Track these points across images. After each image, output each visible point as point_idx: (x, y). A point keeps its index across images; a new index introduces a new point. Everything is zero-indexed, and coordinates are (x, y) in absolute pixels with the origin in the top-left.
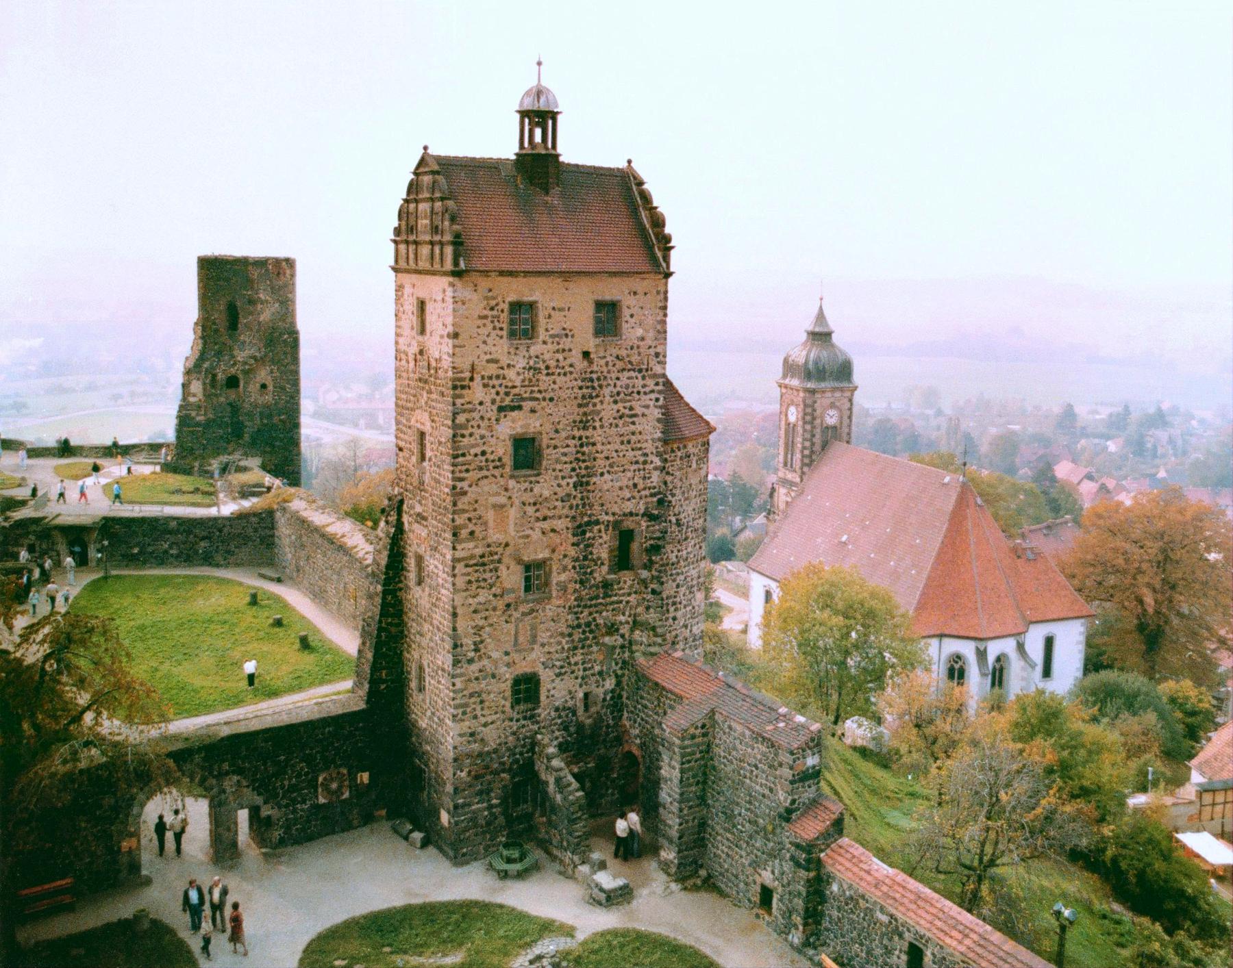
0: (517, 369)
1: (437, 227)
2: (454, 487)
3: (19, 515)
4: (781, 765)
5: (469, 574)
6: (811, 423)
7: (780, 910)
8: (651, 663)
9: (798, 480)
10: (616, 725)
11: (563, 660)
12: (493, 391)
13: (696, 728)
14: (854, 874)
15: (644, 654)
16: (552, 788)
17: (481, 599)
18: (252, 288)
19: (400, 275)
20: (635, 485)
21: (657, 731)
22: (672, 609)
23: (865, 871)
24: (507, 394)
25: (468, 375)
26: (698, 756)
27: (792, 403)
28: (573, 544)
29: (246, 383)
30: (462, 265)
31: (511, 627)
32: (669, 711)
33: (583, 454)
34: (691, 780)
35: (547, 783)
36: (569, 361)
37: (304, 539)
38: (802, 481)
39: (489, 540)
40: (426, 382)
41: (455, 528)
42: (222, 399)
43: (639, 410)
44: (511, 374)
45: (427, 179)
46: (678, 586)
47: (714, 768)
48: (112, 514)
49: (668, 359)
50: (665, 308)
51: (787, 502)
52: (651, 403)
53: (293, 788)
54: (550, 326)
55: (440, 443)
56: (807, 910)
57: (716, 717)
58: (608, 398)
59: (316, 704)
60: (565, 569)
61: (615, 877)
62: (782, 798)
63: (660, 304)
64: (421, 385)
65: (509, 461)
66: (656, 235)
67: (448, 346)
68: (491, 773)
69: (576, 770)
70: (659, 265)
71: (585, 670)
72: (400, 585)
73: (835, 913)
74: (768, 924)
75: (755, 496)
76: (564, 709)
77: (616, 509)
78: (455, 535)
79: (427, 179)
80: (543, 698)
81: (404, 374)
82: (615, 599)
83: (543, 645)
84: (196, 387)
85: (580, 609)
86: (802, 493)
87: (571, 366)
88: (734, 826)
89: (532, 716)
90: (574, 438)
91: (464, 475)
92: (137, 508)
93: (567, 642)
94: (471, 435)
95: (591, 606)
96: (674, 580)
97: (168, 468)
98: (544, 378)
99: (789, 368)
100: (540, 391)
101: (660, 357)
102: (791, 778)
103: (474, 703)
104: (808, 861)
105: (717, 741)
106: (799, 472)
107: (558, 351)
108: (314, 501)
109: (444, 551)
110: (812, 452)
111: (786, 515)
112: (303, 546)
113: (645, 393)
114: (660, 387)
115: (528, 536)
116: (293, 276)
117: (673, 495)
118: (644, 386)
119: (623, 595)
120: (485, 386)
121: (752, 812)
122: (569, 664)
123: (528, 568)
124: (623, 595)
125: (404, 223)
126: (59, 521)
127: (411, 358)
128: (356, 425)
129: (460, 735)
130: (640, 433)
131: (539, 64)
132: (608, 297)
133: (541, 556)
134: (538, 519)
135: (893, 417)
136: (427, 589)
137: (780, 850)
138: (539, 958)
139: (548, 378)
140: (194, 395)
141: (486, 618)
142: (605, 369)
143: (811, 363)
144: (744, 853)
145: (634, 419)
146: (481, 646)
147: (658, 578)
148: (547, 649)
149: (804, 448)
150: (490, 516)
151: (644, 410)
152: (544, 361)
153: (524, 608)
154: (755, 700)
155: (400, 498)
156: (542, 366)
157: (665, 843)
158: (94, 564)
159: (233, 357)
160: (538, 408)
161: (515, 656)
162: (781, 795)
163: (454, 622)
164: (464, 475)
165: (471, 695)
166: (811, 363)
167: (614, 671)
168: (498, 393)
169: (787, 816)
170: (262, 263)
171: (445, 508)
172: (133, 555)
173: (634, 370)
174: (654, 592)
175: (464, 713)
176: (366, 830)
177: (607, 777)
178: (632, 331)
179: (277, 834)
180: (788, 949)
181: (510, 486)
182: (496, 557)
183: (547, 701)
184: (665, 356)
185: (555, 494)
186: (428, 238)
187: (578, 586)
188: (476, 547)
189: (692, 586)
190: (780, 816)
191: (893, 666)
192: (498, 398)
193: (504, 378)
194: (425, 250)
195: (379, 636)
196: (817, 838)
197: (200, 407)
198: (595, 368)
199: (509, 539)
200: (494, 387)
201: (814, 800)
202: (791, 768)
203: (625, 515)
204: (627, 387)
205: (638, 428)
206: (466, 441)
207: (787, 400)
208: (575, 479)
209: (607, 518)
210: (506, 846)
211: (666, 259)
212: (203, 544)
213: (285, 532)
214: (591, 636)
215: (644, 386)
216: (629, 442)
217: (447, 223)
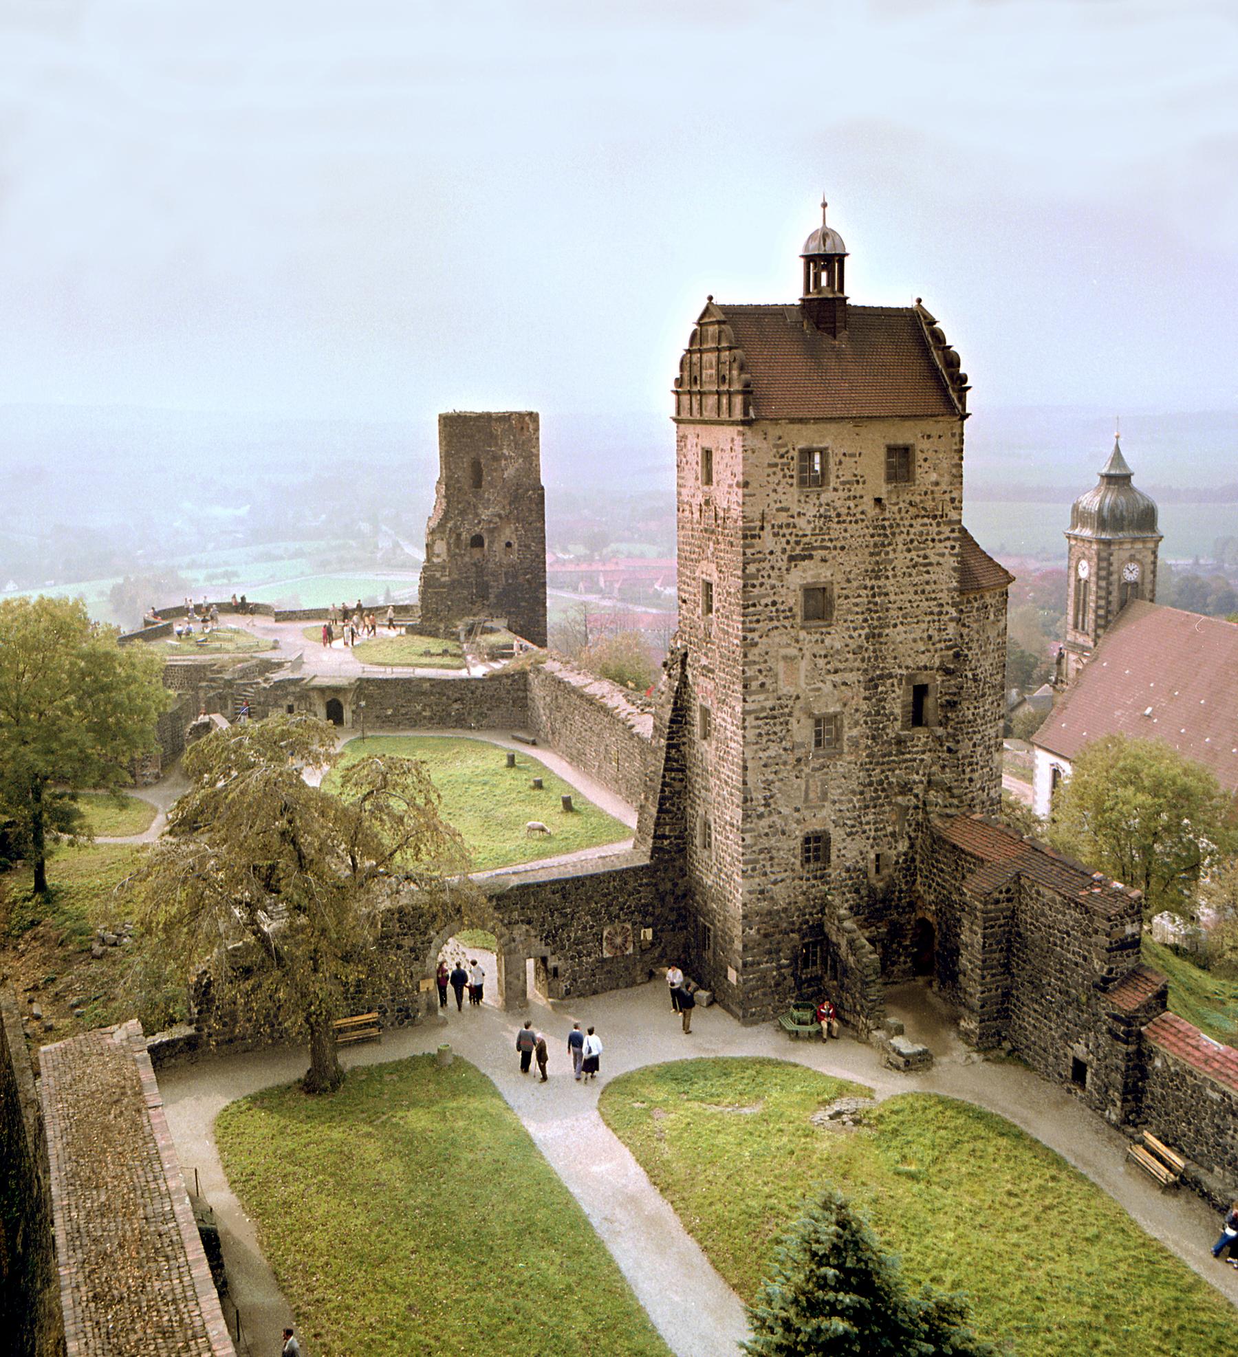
0: (807, 517)
1: (724, 377)
2: (745, 638)
3: (277, 676)
4: (1096, 932)
5: (759, 727)
6: (1107, 578)
7: (1095, 1084)
8: (948, 825)
9: (1091, 644)
10: (910, 890)
11: (855, 819)
12: (784, 540)
13: (1001, 892)
14: (1180, 1049)
15: (940, 816)
16: (844, 950)
17: (771, 753)
18: (496, 445)
19: (682, 426)
20: (930, 637)
21: (955, 897)
22: (968, 770)
23: (1193, 1046)
24: (798, 543)
25: (758, 524)
26: (1002, 921)
27: (1084, 556)
28: (865, 698)
29: (491, 542)
30: (752, 415)
31: (801, 782)
32: (968, 875)
33: (876, 604)
34: (995, 947)
35: (838, 946)
36: (860, 509)
37: (560, 700)
38: (1095, 645)
39: (780, 693)
40: (713, 532)
41: (745, 679)
42: (467, 559)
43: (933, 559)
44: (801, 522)
45: (713, 329)
46: (974, 745)
47: (1019, 935)
48: (365, 676)
49: (964, 504)
50: (962, 450)
51: (1078, 670)
52: (947, 551)
53: (578, 942)
54: (840, 473)
55: (729, 594)
56: (1126, 1085)
57: (1022, 882)
58: (900, 546)
59: (600, 857)
60: (857, 723)
61: (913, 1042)
62: (1099, 966)
63: (955, 447)
64: (706, 535)
65: (798, 610)
66: (951, 376)
67: (737, 495)
68: (780, 932)
69: (867, 934)
70: (955, 407)
71: (876, 830)
72: (684, 740)
73: (1158, 1091)
74: (1081, 1099)
75: (1035, 666)
76: (855, 870)
77: (910, 662)
78: (745, 687)
79: (713, 329)
80: (833, 857)
81: (688, 526)
82: (908, 756)
83: (834, 802)
84: (440, 547)
85: (871, 767)
86: (1095, 660)
87: (863, 513)
88: (1042, 996)
89: (822, 877)
90: (866, 588)
91: (754, 625)
92: (389, 670)
93: (859, 801)
94: (762, 585)
95: (883, 764)
96: (970, 739)
97: (412, 630)
98: (835, 526)
99: (1080, 516)
100: (831, 540)
101: (956, 503)
102: (1107, 945)
103: (764, 859)
104: (1128, 1034)
105: (1023, 907)
106: (1092, 635)
107: (849, 498)
108: (568, 662)
109: (733, 704)
110: (1108, 612)
111: (1077, 684)
112: (559, 708)
113: (940, 541)
114: (956, 534)
115: (819, 689)
116: (537, 429)
117: (970, 649)
118: (939, 533)
119: (917, 753)
120: (776, 535)
121: (1062, 981)
122: (861, 823)
123: (818, 722)
124: (917, 753)
125: (686, 374)
126: (316, 682)
127: (696, 509)
128: (575, 589)
129: (750, 892)
130: (935, 582)
131: (825, 205)
132: (900, 442)
133: (831, 710)
134: (829, 672)
135: (1200, 574)
136: (714, 742)
137: (1095, 1022)
138: (839, 1114)
139: (838, 526)
140: (438, 556)
141: (776, 773)
142: (898, 516)
143: (1105, 510)
144: (1053, 1026)
145: (929, 568)
146: (771, 801)
147: (954, 736)
148: (838, 806)
149: (1098, 607)
150: (780, 667)
151: (938, 558)
152: (835, 509)
153: (816, 763)
154: (1066, 865)
155: (683, 651)
156: (833, 514)
157: (966, 1012)
158: (350, 725)
159: (477, 515)
160: (829, 557)
161: (807, 813)
162: (1097, 964)
163: (745, 776)
164: (754, 625)
165: (761, 851)
166: (1105, 510)
167: (907, 833)
168: (788, 542)
169: (1104, 985)
170: (505, 418)
171: (735, 660)
172: (386, 717)
173: (928, 517)
174: (950, 750)
175: (754, 869)
176: (649, 986)
177: (900, 944)
178: (925, 476)
179: (563, 985)
180: (1104, 1126)
181: (801, 638)
182: (786, 710)
183: (838, 861)
184: (961, 502)
185: (847, 646)
186: (715, 388)
187: (869, 742)
188: (766, 699)
189: (990, 747)
190: (1096, 986)
191: (1211, 853)
192: (788, 547)
193: (795, 527)
194: (711, 401)
195: (663, 791)
196: (1137, 1010)
197: (444, 568)
198: (887, 515)
199: (799, 691)
200: (784, 536)
201: (1134, 971)
202: (1108, 935)
203: (919, 668)
204: (921, 534)
205: (933, 577)
206: (756, 591)
207: (1077, 552)
208: (867, 630)
209: (900, 671)
210: (797, 1007)
211: (962, 400)
212: (456, 706)
213: (539, 693)
214: (883, 795)
215: (939, 533)
216: (923, 592)
217: (735, 373)
